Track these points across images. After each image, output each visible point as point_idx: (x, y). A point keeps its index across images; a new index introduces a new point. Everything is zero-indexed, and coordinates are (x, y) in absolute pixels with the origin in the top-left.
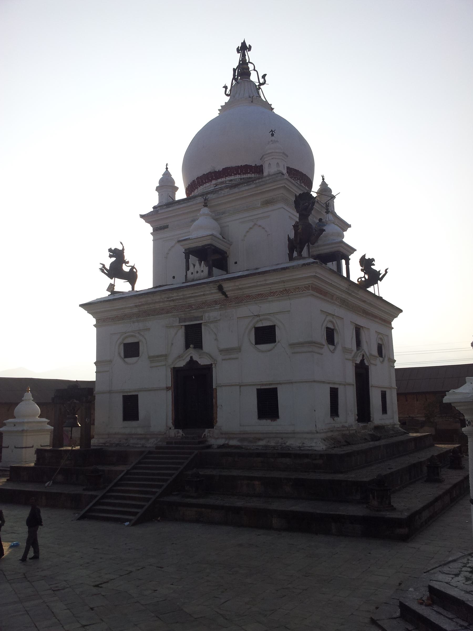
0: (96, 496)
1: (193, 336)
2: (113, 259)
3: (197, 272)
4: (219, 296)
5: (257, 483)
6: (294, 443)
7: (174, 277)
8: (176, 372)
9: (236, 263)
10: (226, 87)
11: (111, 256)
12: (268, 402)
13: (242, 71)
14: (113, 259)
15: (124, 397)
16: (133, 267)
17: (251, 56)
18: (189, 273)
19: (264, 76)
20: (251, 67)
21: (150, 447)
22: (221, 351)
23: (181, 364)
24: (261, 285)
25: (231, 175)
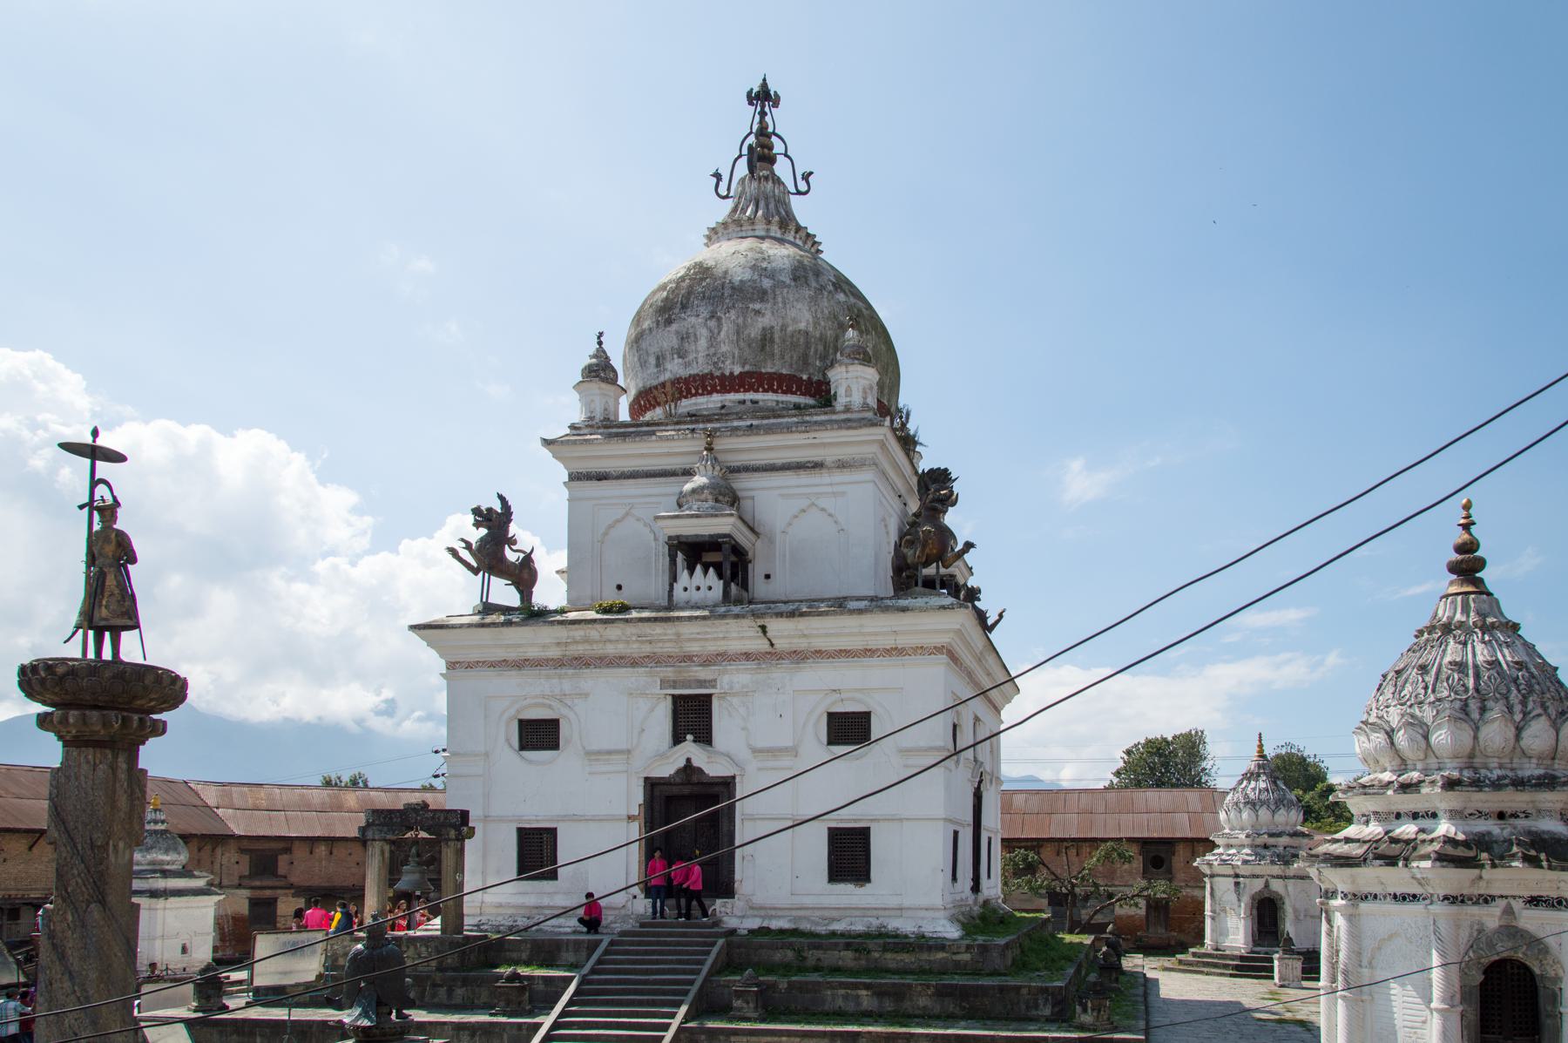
0: (538, 1026)
1: (692, 717)
2: (483, 531)
3: (698, 588)
4: (762, 645)
5: (864, 992)
6: (906, 926)
7: (619, 587)
8: (651, 785)
9: (768, 577)
10: (718, 176)
11: (477, 525)
12: (850, 855)
13: (761, 154)
14: (483, 531)
15: (522, 833)
16: (528, 559)
17: (779, 119)
18: (678, 587)
19: (806, 177)
20: (778, 147)
21: (782, 931)
22: (756, 751)
23: (666, 770)
24: (851, 634)
25: (757, 391)
